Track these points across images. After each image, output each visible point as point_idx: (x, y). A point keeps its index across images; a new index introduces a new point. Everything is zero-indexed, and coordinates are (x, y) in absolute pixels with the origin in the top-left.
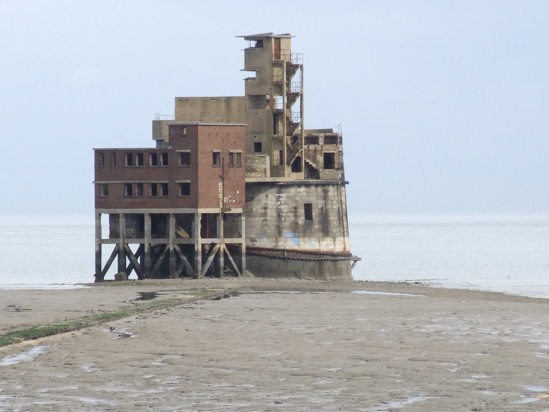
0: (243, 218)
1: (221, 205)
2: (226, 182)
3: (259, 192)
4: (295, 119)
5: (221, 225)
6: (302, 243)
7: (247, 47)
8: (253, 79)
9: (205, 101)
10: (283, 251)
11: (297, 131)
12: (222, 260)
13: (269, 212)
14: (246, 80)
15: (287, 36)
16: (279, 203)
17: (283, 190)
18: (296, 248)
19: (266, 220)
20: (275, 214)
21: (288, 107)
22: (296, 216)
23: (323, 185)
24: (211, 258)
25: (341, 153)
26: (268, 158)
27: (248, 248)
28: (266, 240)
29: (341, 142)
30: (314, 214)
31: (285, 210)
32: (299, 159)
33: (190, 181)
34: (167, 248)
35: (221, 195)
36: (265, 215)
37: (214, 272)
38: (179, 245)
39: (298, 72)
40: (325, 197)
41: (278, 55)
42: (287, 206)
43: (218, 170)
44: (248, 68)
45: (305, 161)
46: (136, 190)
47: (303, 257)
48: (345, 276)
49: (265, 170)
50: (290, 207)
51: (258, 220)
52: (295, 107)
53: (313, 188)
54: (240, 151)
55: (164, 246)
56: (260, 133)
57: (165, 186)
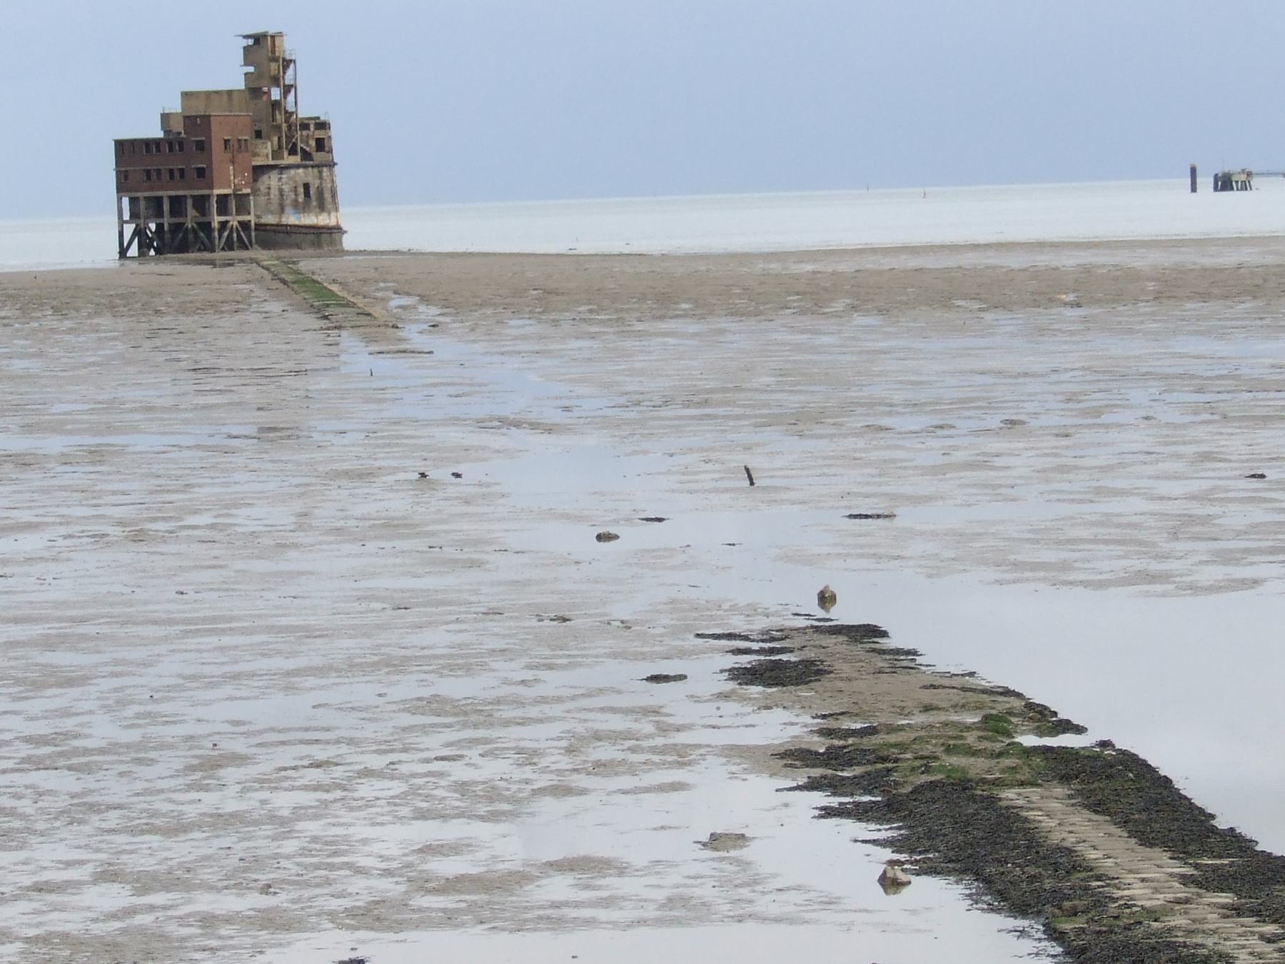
0: (251, 197)
2: (236, 165)
3: (263, 174)
4: (291, 108)
5: (233, 205)
6: (302, 219)
7: (246, 45)
8: (252, 73)
9: (209, 95)
10: (286, 225)
12: (235, 235)
14: (246, 74)
15: (281, 34)
17: (284, 172)
18: (297, 223)
19: (269, 199)
20: (277, 193)
21: (285, 98)
22: (296, 195)
23: (318, 166)
24: (226, 234)
25: (330, 137)
26: (269, 144)
27: (256, 224)
28: (270, 217)
29: (330, 128)
30: (311, 192)
31: (287, 190)
32: (295, 145)
33: (205, 166)
34: (185, 226)
35: (232, 178)
36: (269, 194)
37: (229, 246)
38: (196, 223)
39: (292, 65)
40: (321, 178)
41: (273, 51)
42: (288, 186)
43: (229, 155)
44: (246, 64)
45: (301, 148)
46: (154, 176)
47: (306, 231)
48: (338, 247)
49: (267, 155)
51: (263, 199)
52: (291, 97)
53: (310, 169)
54: (246, 138)
56: (260, 121)
57: (182, 171)
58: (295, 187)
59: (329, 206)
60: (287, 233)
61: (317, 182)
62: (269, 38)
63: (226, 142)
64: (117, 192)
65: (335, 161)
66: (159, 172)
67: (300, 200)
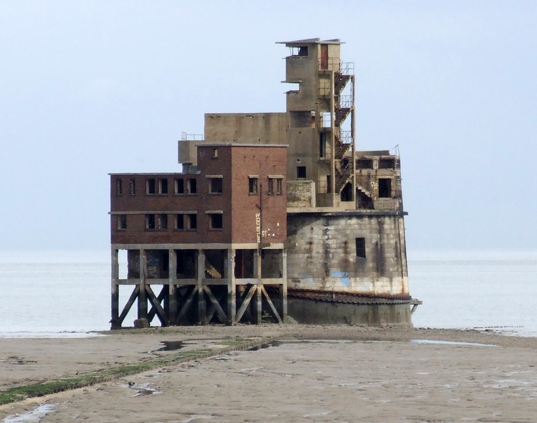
0: (285, 255)
1: (258, 240)
3: (303, 224)
4: (345, 139)
6: (353, 284)
7: (289, 55)
8: (296, 92)
10: (331, 293)
11: (348, 153)
12: (259, 303)
13: (314, 248)
14: (288, 93)
15: (336, 43)
16: (326, 237)
17: (331, 222)
18: (346, 289)
20: (321, 250)
21: (337, 125)
22: (346, 253)
23: (378, 216)
24: (247, 301)
25: (398, 178)
26: (313, 185)
27: (290, 290)
28: (311, 280)
29: (399, 166)
30: (367, 250)
31: (334, 246)
33: (222, 212)
34: (195, 289)
35: (258, 228)
36: (310, 251)
38: (209, 286)
39: (349, 84)
40: (381, 231)
41: (325, 64)
42: (335, 241)
43: (255, 199)
44: (290, 79)
45: (357, 188)
46: (159, 222)
47: (360, 300)
48: (403, 323)
49: (310, 199)
50: (339, 241)
51: (301, 257)
52: (346, 125)
54: (280, 176)
55: (193, 287)
56: (304, 155)
57: (193, 217)
58: (346, 243)
59: (391, 268)
60: (332, 302)
61: (375, 237)
62: (319, 46)
63: (252, 181)
64: (112, 243)
65: (405, 210)
66: (164, 217)
67: (351, 260)
